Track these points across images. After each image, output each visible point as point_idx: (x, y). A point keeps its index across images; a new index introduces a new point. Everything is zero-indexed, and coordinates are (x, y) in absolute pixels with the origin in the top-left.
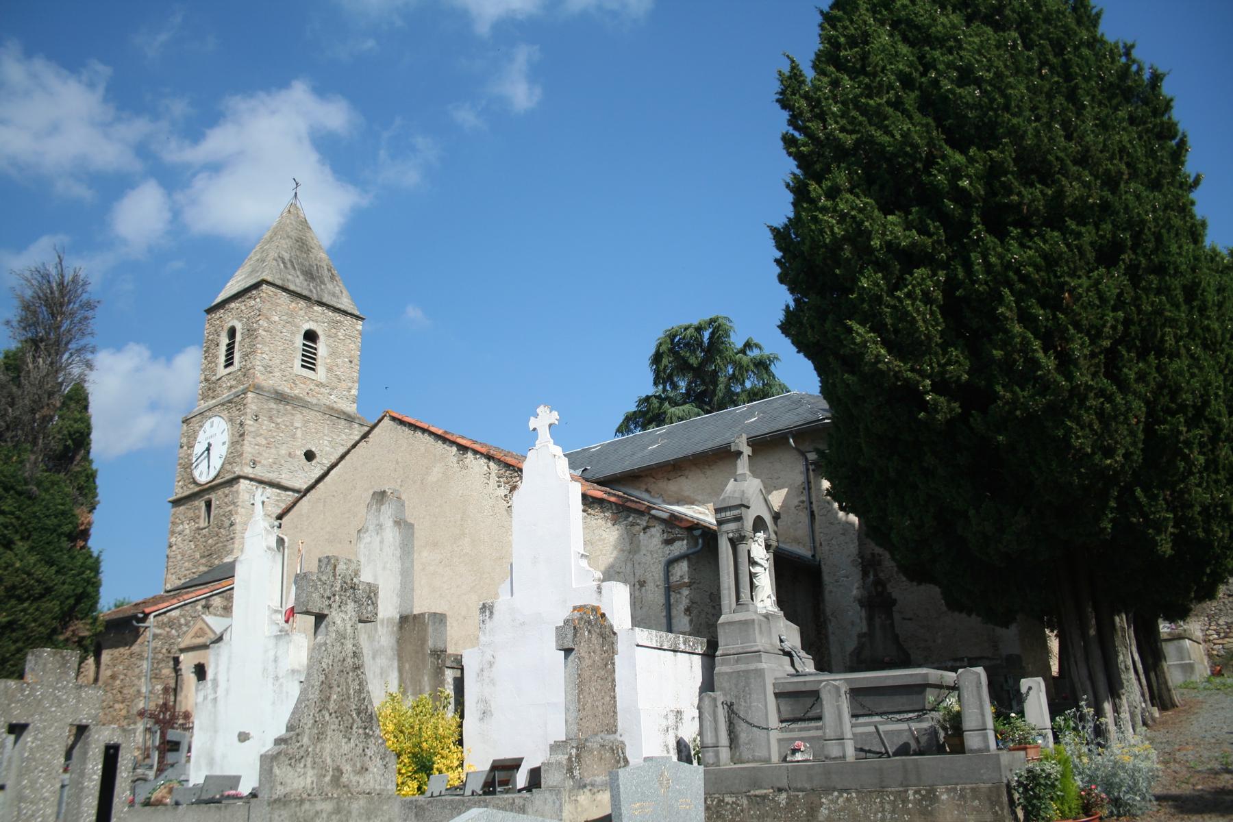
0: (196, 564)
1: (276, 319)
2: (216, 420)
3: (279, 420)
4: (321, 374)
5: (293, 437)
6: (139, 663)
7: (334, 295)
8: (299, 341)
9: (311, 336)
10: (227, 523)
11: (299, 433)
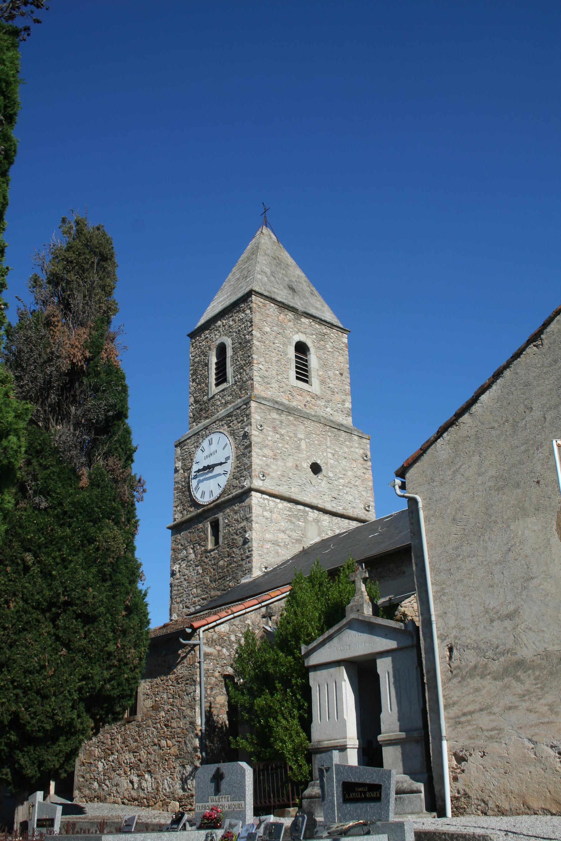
0: (205, 588)
1: (268, 329)
2: (215, 437)
3: (283, 432)
4: (315, 386)
5: (298, 448)
6: (190, 689)
7: (317, 309)
8: (291, 352)
9: (301, 349)
10: (240, 541)
11: (303, 445)
